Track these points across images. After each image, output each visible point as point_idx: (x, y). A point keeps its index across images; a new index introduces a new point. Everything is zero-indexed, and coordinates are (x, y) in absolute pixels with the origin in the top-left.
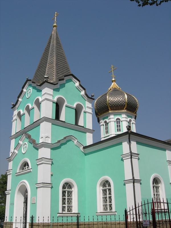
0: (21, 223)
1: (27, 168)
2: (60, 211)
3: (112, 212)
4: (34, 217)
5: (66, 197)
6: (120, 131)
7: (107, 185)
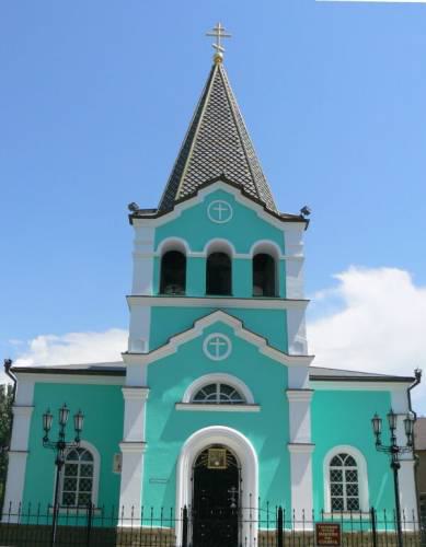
1: (218, 397)
2: (328, 508)
7: (343, 463)
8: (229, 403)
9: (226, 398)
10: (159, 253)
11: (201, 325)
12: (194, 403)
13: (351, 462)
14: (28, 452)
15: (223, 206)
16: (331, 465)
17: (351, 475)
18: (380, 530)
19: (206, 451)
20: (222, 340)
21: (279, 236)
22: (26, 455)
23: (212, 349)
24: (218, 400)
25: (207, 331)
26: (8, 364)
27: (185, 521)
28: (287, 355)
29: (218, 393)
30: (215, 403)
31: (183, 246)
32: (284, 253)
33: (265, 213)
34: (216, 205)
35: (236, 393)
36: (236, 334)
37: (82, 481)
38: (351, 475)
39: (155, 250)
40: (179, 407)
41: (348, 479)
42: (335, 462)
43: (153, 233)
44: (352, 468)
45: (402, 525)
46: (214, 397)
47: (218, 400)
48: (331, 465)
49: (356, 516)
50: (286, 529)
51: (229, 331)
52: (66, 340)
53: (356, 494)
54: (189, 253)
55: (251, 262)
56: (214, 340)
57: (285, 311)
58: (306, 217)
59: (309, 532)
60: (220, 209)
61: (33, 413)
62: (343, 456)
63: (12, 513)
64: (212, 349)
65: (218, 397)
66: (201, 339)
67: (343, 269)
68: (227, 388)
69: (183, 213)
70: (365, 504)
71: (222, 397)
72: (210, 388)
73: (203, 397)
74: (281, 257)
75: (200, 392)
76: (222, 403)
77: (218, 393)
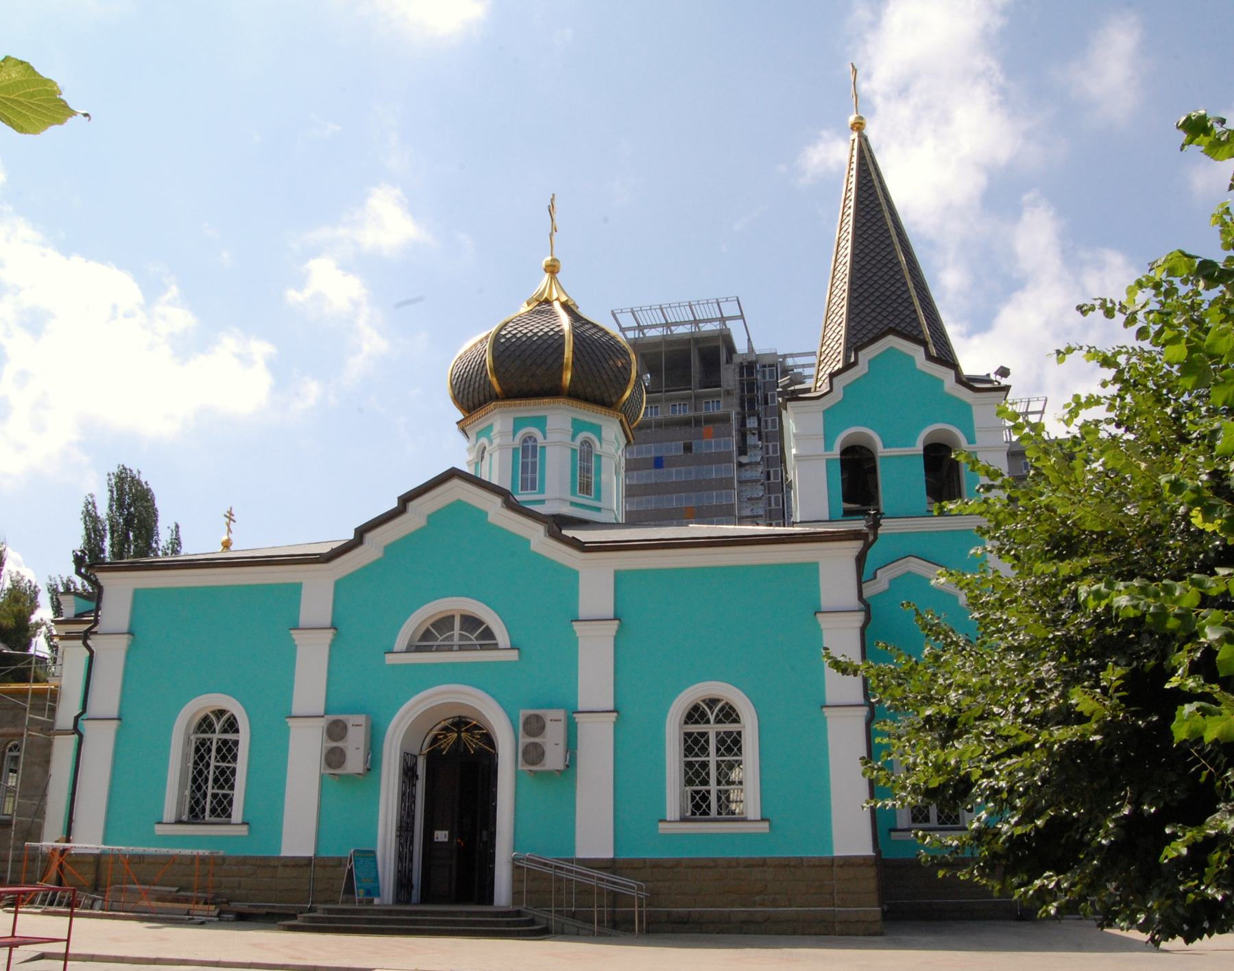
1: (456, 637)
3: (229, 823)
5: (713, 787)
6: (533, 488)
7: (712, 718)
9: (470, 640)
10: (836, 452)
12: (419, 649)
13: (729, 714)
14: (119, 719)
17: (696, 742)
21: (963, 414)
22: (115, 723)
27: (408, 773)
30: (450, 649)
31: (870, 439)
33: (978, 395)
37: (704, 750)
38: (696, 742)
39: (828, 447)
40: (390, 659)
42: (695, 714)
48: (704, 701)
52: (758, 522)
53: (689, 765)
54: (881, 450)
57: (601, 426)
62: (712, 702)
65: (456, 637)
67: (1180, 935)
68: (470, 622)
71: (462, 637)
72: (444, 623)
76: (461, 648)
77: (457, 631)
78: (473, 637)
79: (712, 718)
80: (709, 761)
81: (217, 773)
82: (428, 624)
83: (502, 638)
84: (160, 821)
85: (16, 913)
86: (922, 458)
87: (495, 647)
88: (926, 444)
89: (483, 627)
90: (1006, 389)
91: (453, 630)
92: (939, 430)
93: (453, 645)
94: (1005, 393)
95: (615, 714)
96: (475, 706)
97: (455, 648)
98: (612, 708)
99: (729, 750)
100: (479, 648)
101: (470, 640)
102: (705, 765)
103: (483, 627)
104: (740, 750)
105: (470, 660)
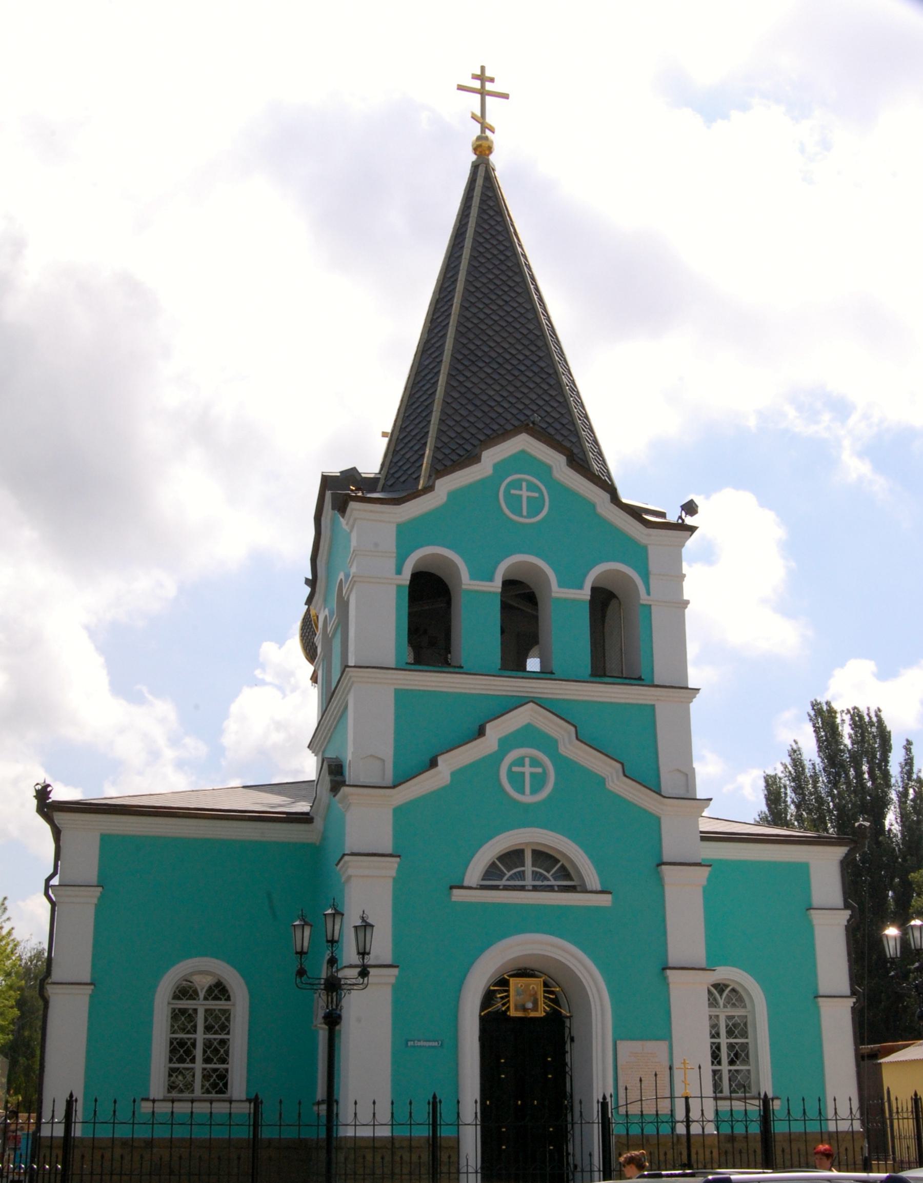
0: (318, 1125)
1: (529, 875)
2: (157, 1085)
4: (440, 1102)
5: (200, 1036)
8: (551, 889)
9: (546, 879)
11: (495, 731)
15: (532, 487)
16: (176, 997)
18: (695, 1129)
19: (503, 983)
20: (535, 762)
23: (517, 780)
24: (529, 881)
25: (507, 744)
26: (42, 794)
28: (659, 794)
29: (528, 867)
30: (522, 888)
32: (648, 593)
34: (517, 485)
35: (563, 868)
36: (562, 750)
37: (208, 1044)
39: (399, 572)
40: (458, 895)
41: (208, 1029)
43: (389, 542)
44: (737, 1012)
45: (324, 1120)
46: (521, 875)
47: (529, 881)
49: (221, 1108)
50: (95, 1136)
51: (548, 744)
53: (224, 1061)
55: (588, 603)
56: (520, 762)
58: (689, 521)
59: (381, 1138)
60: (525, 493)
61: (101, 898)
63: (100, 1118)
64: (539, 782)
65: (529, 875)
66: (495, 760)
68: (544, 858)
69: (453, 495)
70: (238, 1086)
71: (536, 875)
72: (513, 857)
73: (501, 876)
74: (644, 598)
75: (493, 865)
76: (535, 889)
77: (528, 867)
78: (549, 875)
79: (721, 1002)
80: (228, 1039)
81: (711, 999)
82: (563, 861)
83: (593, 880)
84: (147, 1097)
85: (675, 1098)
86: (407, 588)
87: (580, 888)
88: (504, 579)
89: (498, 863)
90: (692, 529)
91: (523, 866)
92: (520, 562)
93: (525, 886)
94: (690, 533)
95: (92, 987)
96: (525, 953)
97: (501, 887)
98: (89, 981)
99: (182, 1043)
100: (556, 888)
101: (546, 879)
102: (207, 1060)
103: (498, 863)
104: (171, 1043)
105: (532, 902)
